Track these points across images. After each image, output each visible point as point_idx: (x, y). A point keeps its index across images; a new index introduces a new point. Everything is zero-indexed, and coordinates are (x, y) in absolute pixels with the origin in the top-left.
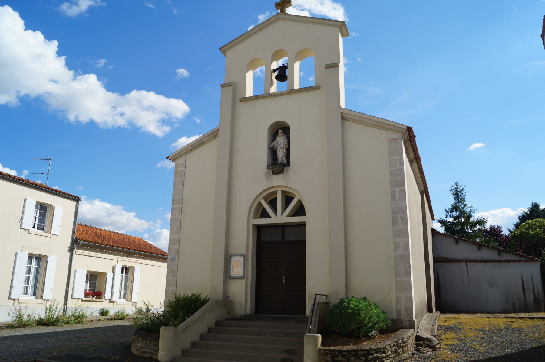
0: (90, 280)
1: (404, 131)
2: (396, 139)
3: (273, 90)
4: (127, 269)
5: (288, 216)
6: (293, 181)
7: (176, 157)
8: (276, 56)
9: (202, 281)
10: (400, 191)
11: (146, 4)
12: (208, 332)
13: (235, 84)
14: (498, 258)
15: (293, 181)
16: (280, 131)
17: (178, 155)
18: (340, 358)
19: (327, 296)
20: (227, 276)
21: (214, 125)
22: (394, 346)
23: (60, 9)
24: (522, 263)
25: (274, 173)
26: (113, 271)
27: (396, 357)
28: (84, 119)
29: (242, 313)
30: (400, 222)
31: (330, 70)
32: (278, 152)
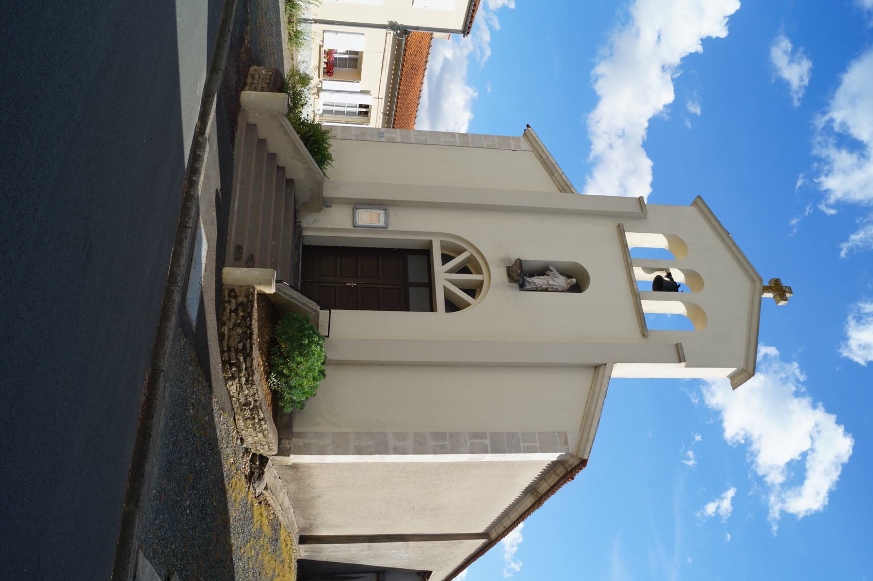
0: (350, 59)
1: (580, 455)
2: (566, 443)
3: (639, 274)
4: (366, 113)
5: (446, 290)
6: (497, 288)
7: (530, 137)
9: (351, 170)
11: (801, 175)
13: (645, 217)
15: (497, 288)
16: (574, 280)
18: (242, 314)
19: (328, 336)
22: (256, 401)
23: (782, 37)
25: (508, 268)
26: (362, 92)
27: (240, 403)
28: (601, 87)
29: (304, 224)
30: (437, 443)
31: (674, 351)
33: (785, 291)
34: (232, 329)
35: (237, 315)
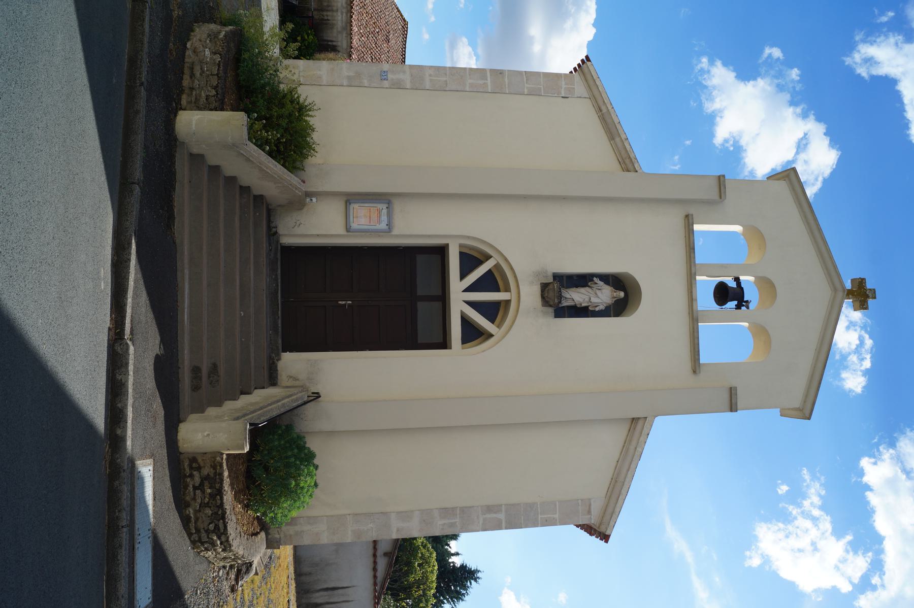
2: (589, 512)
8: (767, 285)
10: (500, 521)
12: (241, 187)
14: (380, 553)
16: (622, 294)
17: (591, 82)
18: (209, 491)
20: (350, 199)
21: (646, 162)
24: (372, 588)
25: (544, 287)
29: (281, 231)
30: (446, 521)
31: (726, 396)
32: (582, 290)
33: (868, 297)
34: (200, 511)
35: (203, 492)
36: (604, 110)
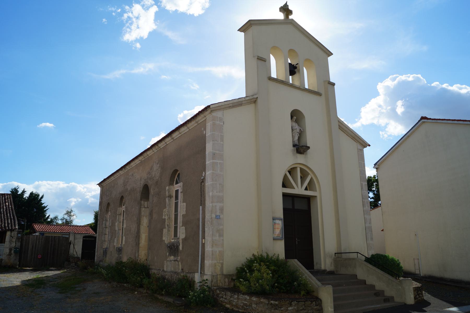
17: (219, 108)
36: (231, 105)
